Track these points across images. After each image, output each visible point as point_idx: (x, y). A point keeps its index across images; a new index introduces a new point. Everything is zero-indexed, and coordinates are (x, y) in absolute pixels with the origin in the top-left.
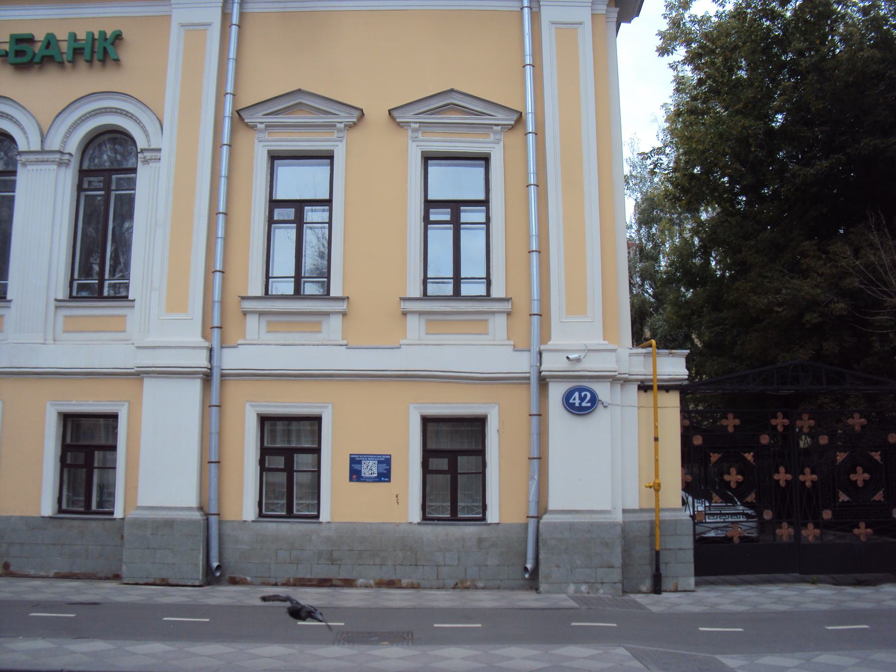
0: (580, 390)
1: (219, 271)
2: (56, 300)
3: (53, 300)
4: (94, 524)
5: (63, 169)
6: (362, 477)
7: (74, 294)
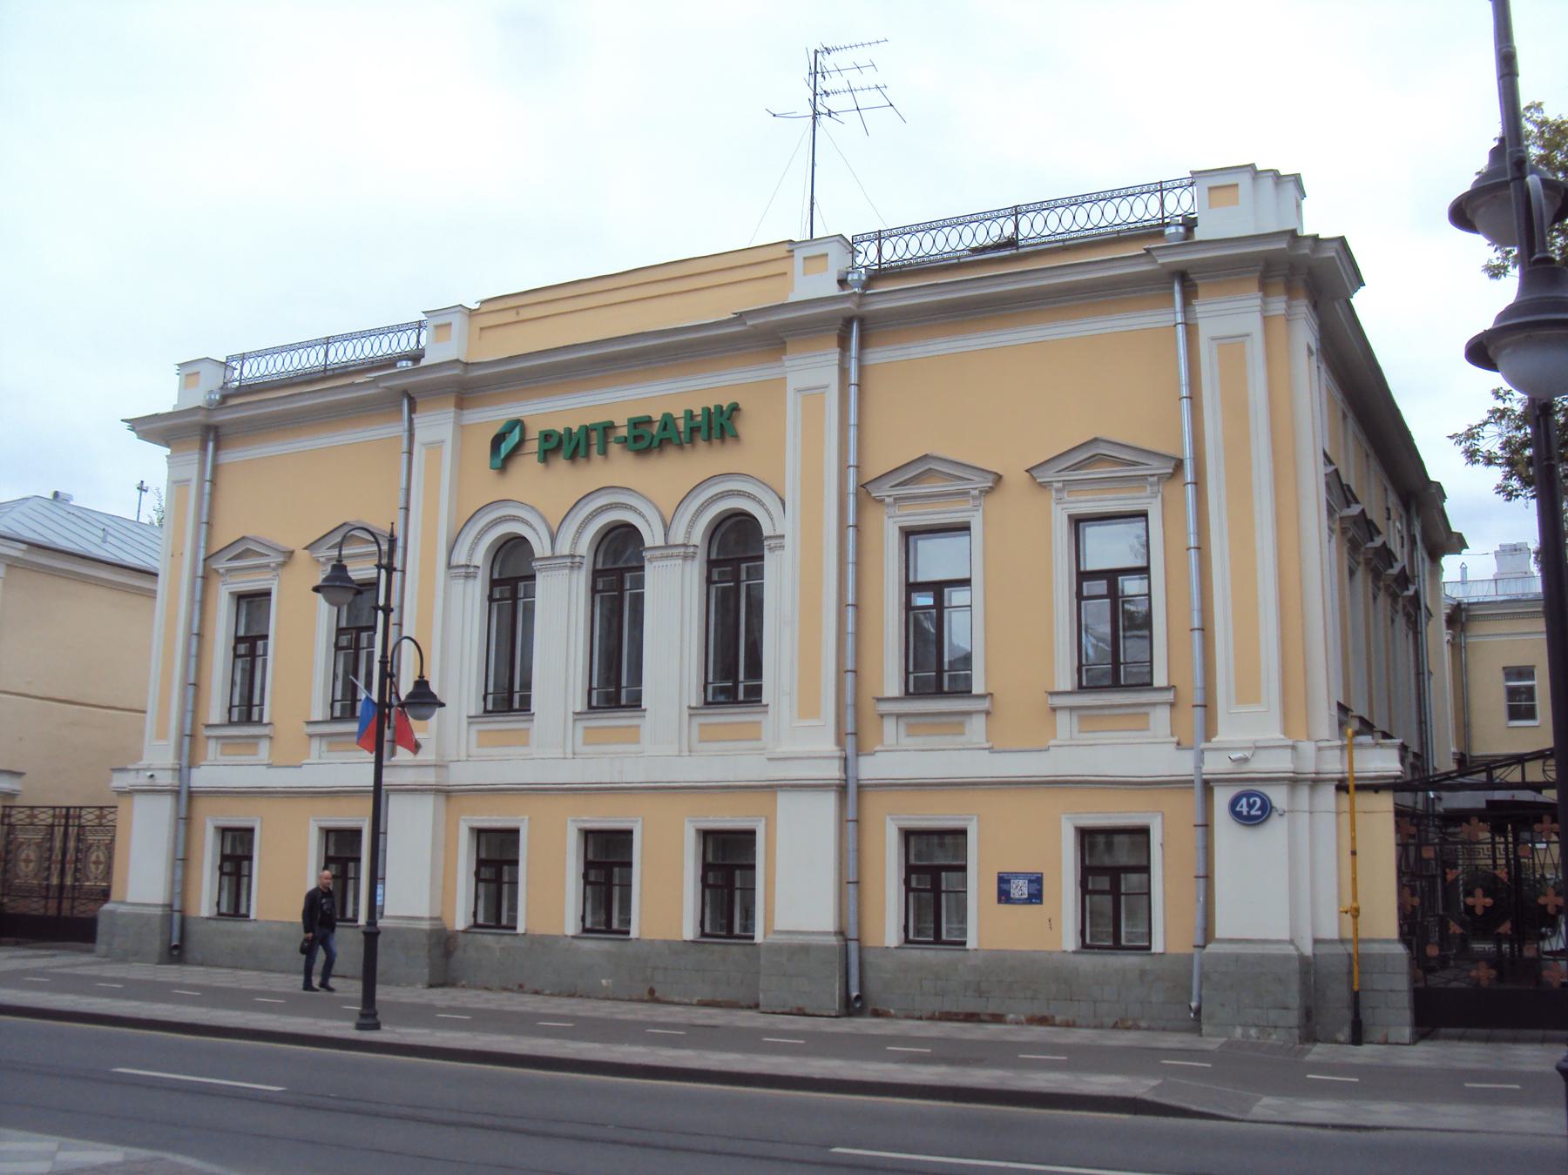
0: (1248, 795)
1: (851, 671)
2: (690, 708)
3: (686, 709)
4: (734, 949)
5: (689, 562)
6: (1011, 899)
7: (710, 699)
